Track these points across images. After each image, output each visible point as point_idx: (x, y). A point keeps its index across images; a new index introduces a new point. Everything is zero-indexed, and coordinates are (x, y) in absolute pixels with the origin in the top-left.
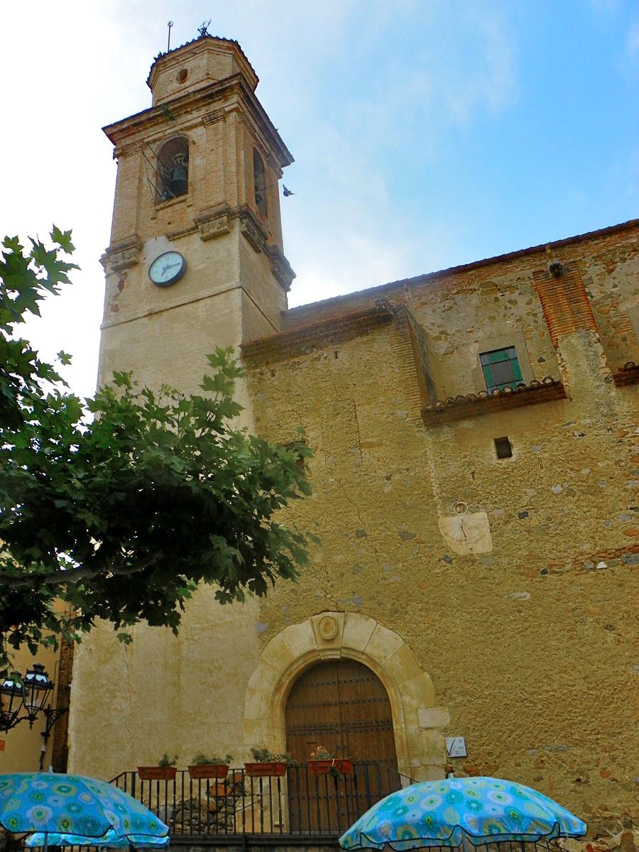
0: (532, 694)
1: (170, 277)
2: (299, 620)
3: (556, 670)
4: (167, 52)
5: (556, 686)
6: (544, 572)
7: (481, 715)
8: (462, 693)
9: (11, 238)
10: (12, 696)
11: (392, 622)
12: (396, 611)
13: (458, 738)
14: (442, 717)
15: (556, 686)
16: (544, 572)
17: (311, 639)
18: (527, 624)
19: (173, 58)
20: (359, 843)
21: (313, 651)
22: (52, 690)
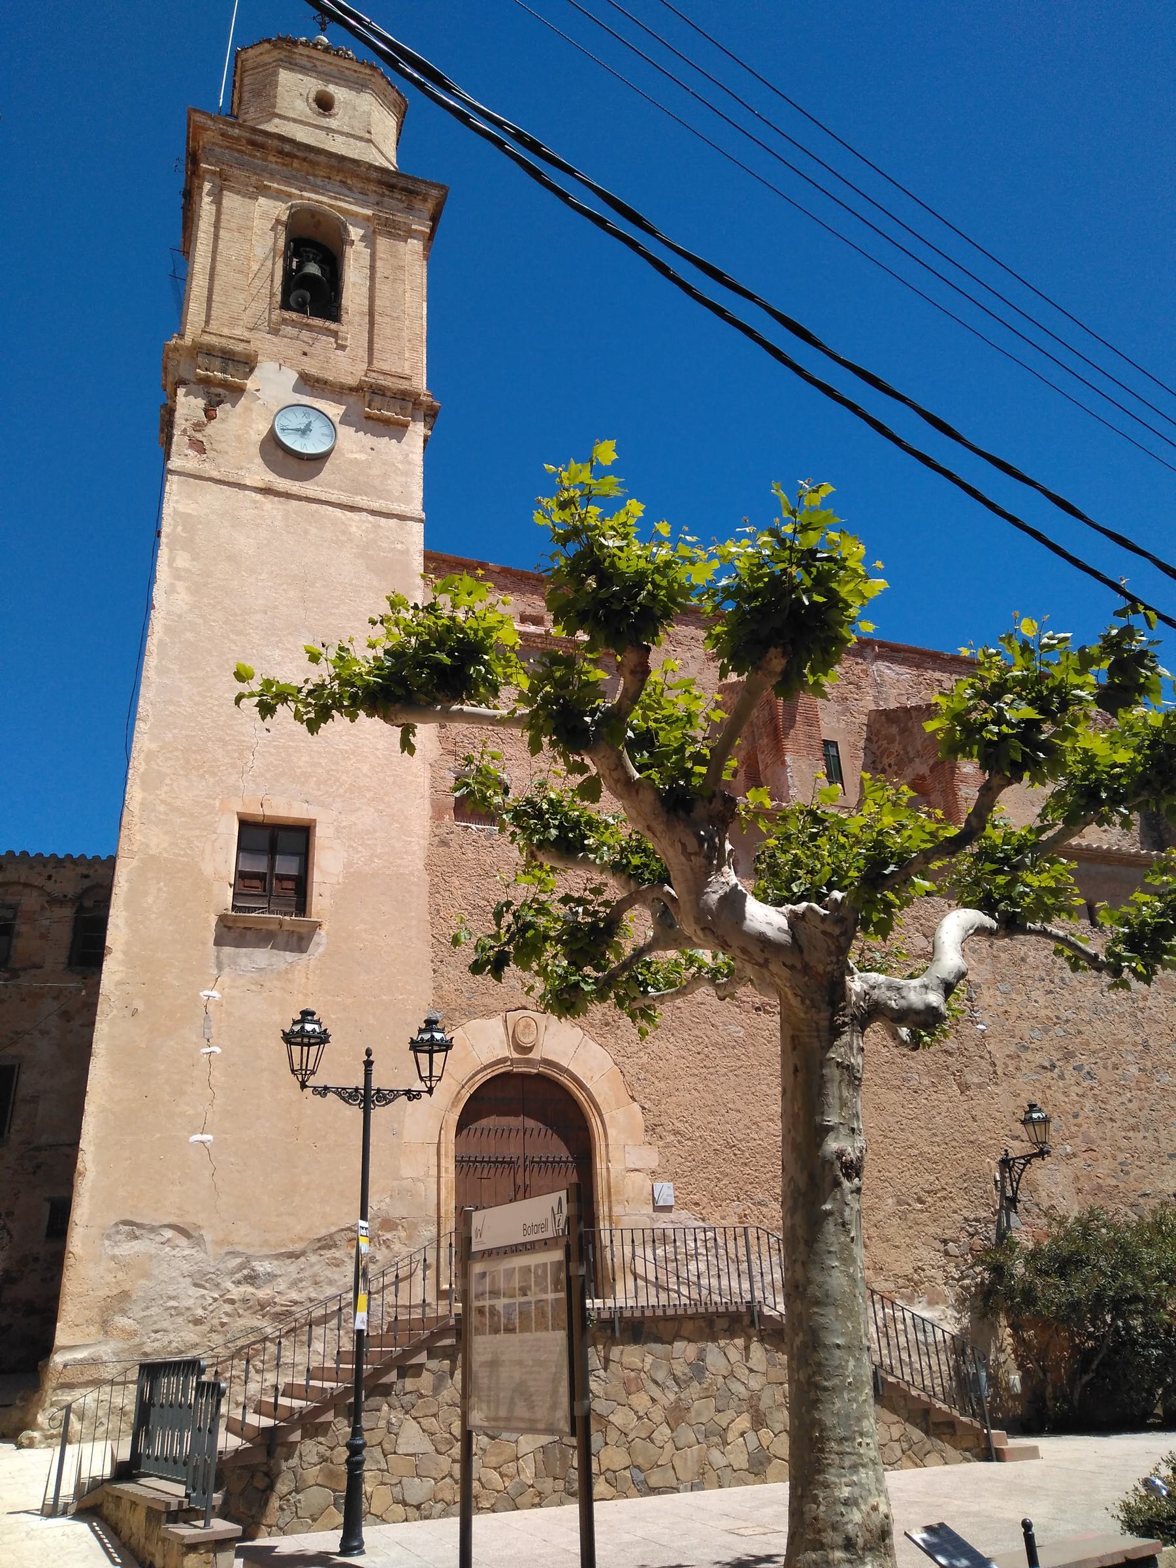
0: (740, 1141)
1: (297, 447)
2: (488, 1013)
3: (764, 1118)
4: (104, 858)
5: (763, 1135)
6: (758, 1009)
7: (690, 1159)
8: (676, 1133)
9: (32, 854)
10: (431, 1053)
11: (602, 1035)
12: (607, 1024)
13: (667, 1184)
14: (650, 1158)
15: (763, 1135)
16: (758, 1009)
17: (502, 1042)
18: (739, 1063)
19: (308, 56)
20: (477, 1268)
21: (503, 1060)
22: (530, 1383)
